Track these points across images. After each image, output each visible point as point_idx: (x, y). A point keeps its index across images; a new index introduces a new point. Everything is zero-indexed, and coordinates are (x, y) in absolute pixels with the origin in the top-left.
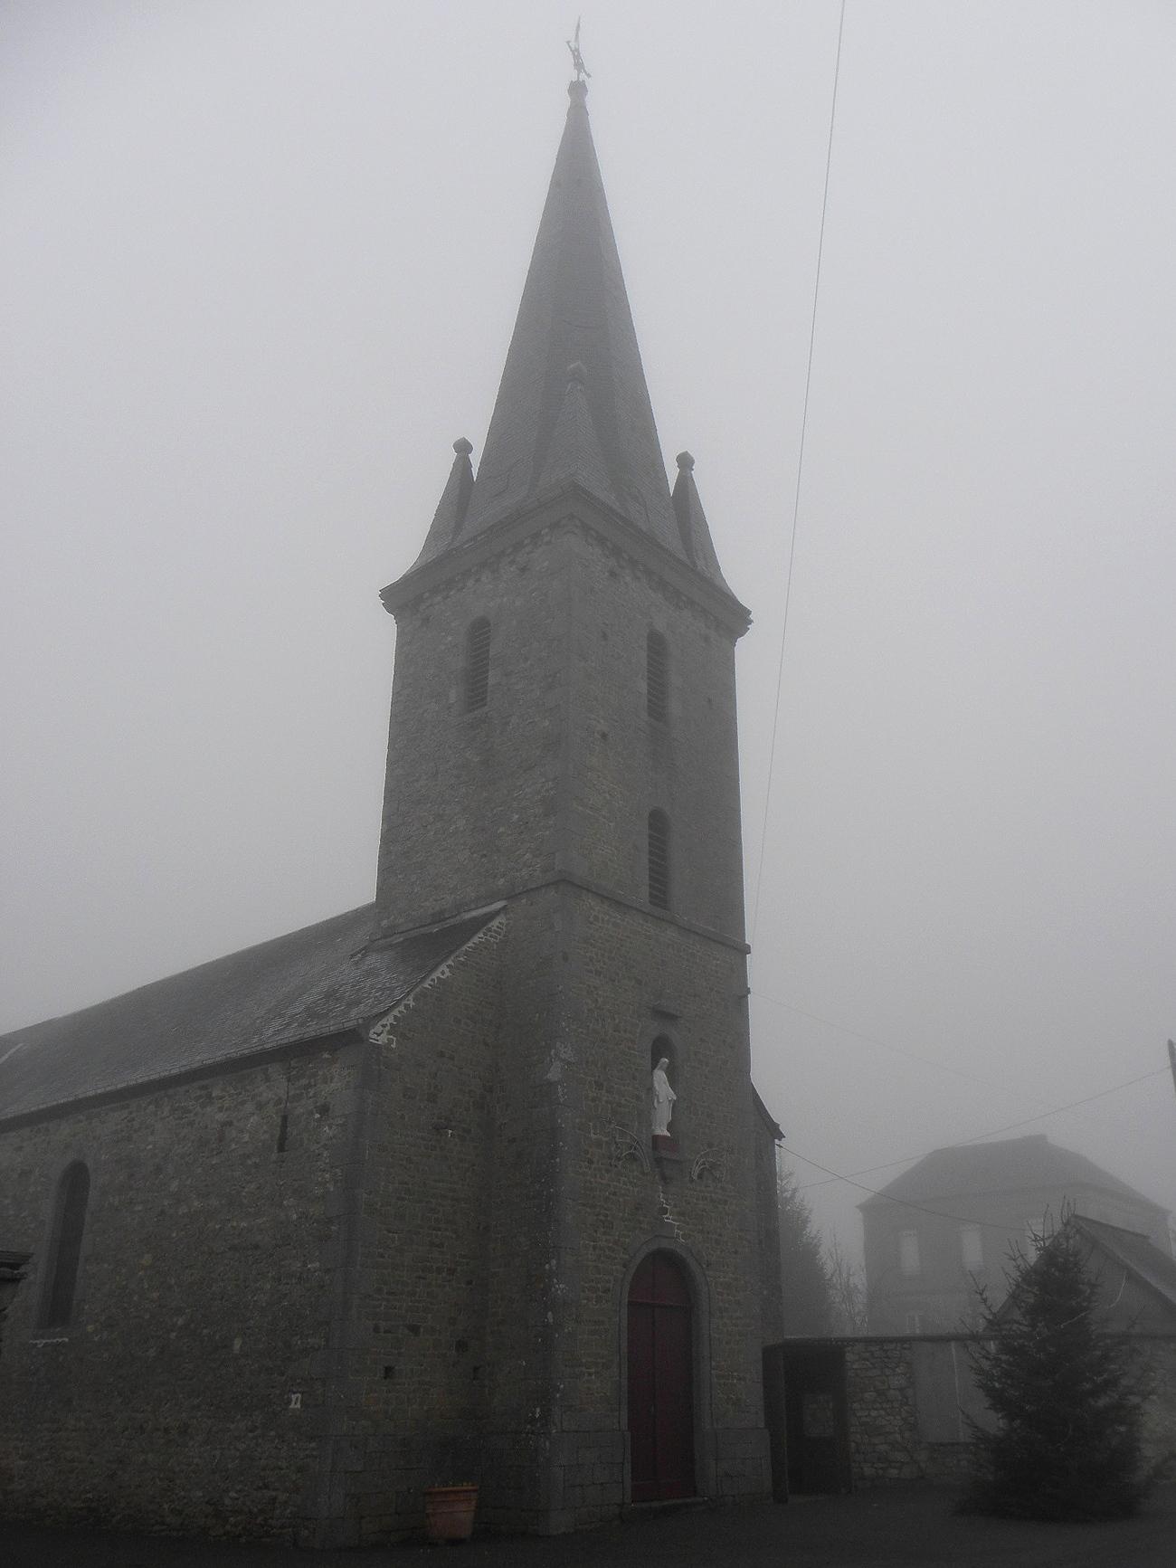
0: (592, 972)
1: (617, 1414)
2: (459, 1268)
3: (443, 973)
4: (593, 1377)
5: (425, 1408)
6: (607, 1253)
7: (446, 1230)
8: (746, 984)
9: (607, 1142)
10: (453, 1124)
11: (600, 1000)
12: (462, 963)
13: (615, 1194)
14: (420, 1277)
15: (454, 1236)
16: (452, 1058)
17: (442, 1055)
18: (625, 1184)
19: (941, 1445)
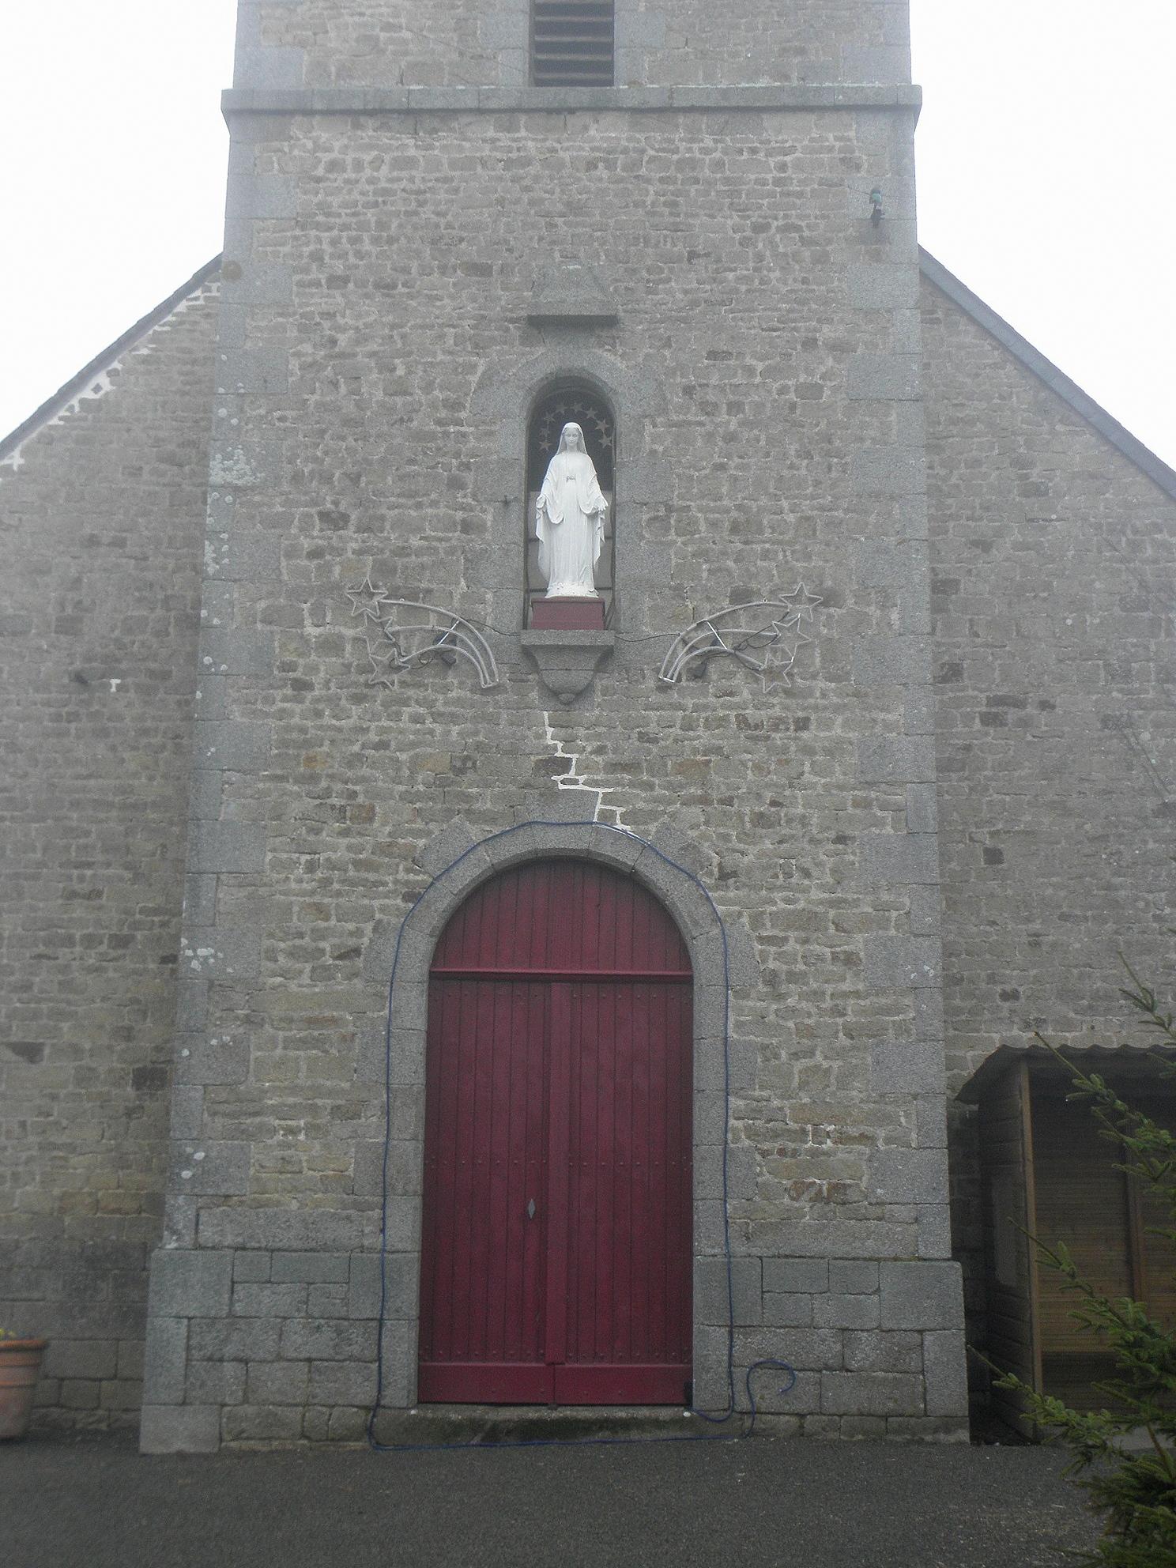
0: (318, 284)
1: (376, 1213)
2: (139, 935)
3: (97, 389)
4: (302, 1137)
5: (56, 1191)
6: (351, 873)
7: (108, 865)
8: (908, 79)
9: (356, 640)
10: (124, 666)
11: (343, 339)
12: (145, 360)
13: (382, 745)
14: (40, 956)
15: (128, 875)
16: (119, 543)
17: (93, 541)
18: (416, 719)
19: (1031, 1328)
